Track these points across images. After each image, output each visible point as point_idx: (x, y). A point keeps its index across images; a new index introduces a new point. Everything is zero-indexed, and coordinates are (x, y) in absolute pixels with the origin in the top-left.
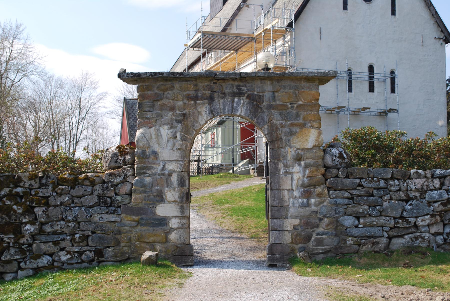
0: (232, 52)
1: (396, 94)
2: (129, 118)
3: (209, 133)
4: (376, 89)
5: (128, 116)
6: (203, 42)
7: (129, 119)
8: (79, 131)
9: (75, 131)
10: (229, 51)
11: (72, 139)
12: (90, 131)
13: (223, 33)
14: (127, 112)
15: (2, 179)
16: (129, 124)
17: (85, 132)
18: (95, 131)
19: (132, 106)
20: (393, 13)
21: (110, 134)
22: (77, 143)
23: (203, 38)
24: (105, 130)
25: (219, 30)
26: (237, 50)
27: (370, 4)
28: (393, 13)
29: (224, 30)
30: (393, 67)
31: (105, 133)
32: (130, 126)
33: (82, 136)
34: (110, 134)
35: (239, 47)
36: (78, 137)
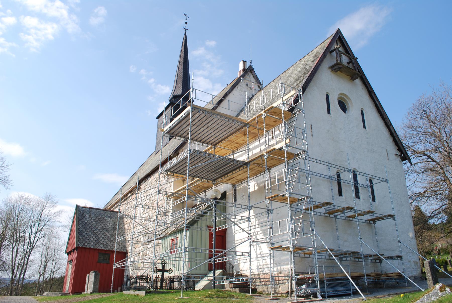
0: (210, 146)
2: (78, 224)
3: (169, 239)
4: (361, 196)
5: (78, 221)
6: (187, 123)
7: (78, 225)
8: (36, 239)
9: (32, 239)
10: (207, 145)
11: (29, 245)
12: (46, 240)
13: (213, 112)
14: (78, 218)
15: (450, 167)
16: (78, 229)
17: (41, 240)
18: (49, 240)
19: (83, 214)
21: (61, 243)
22: (32, 248)
23: (192, 112)
24: (57, 240)
25: (210, 107)
26: (215, 145)
29: (215, 108)
31: (57, 243)
32: (79, 231)
33: (38, 243)
34: (61, 243)
35: (216, 142)
36: (34, 244)
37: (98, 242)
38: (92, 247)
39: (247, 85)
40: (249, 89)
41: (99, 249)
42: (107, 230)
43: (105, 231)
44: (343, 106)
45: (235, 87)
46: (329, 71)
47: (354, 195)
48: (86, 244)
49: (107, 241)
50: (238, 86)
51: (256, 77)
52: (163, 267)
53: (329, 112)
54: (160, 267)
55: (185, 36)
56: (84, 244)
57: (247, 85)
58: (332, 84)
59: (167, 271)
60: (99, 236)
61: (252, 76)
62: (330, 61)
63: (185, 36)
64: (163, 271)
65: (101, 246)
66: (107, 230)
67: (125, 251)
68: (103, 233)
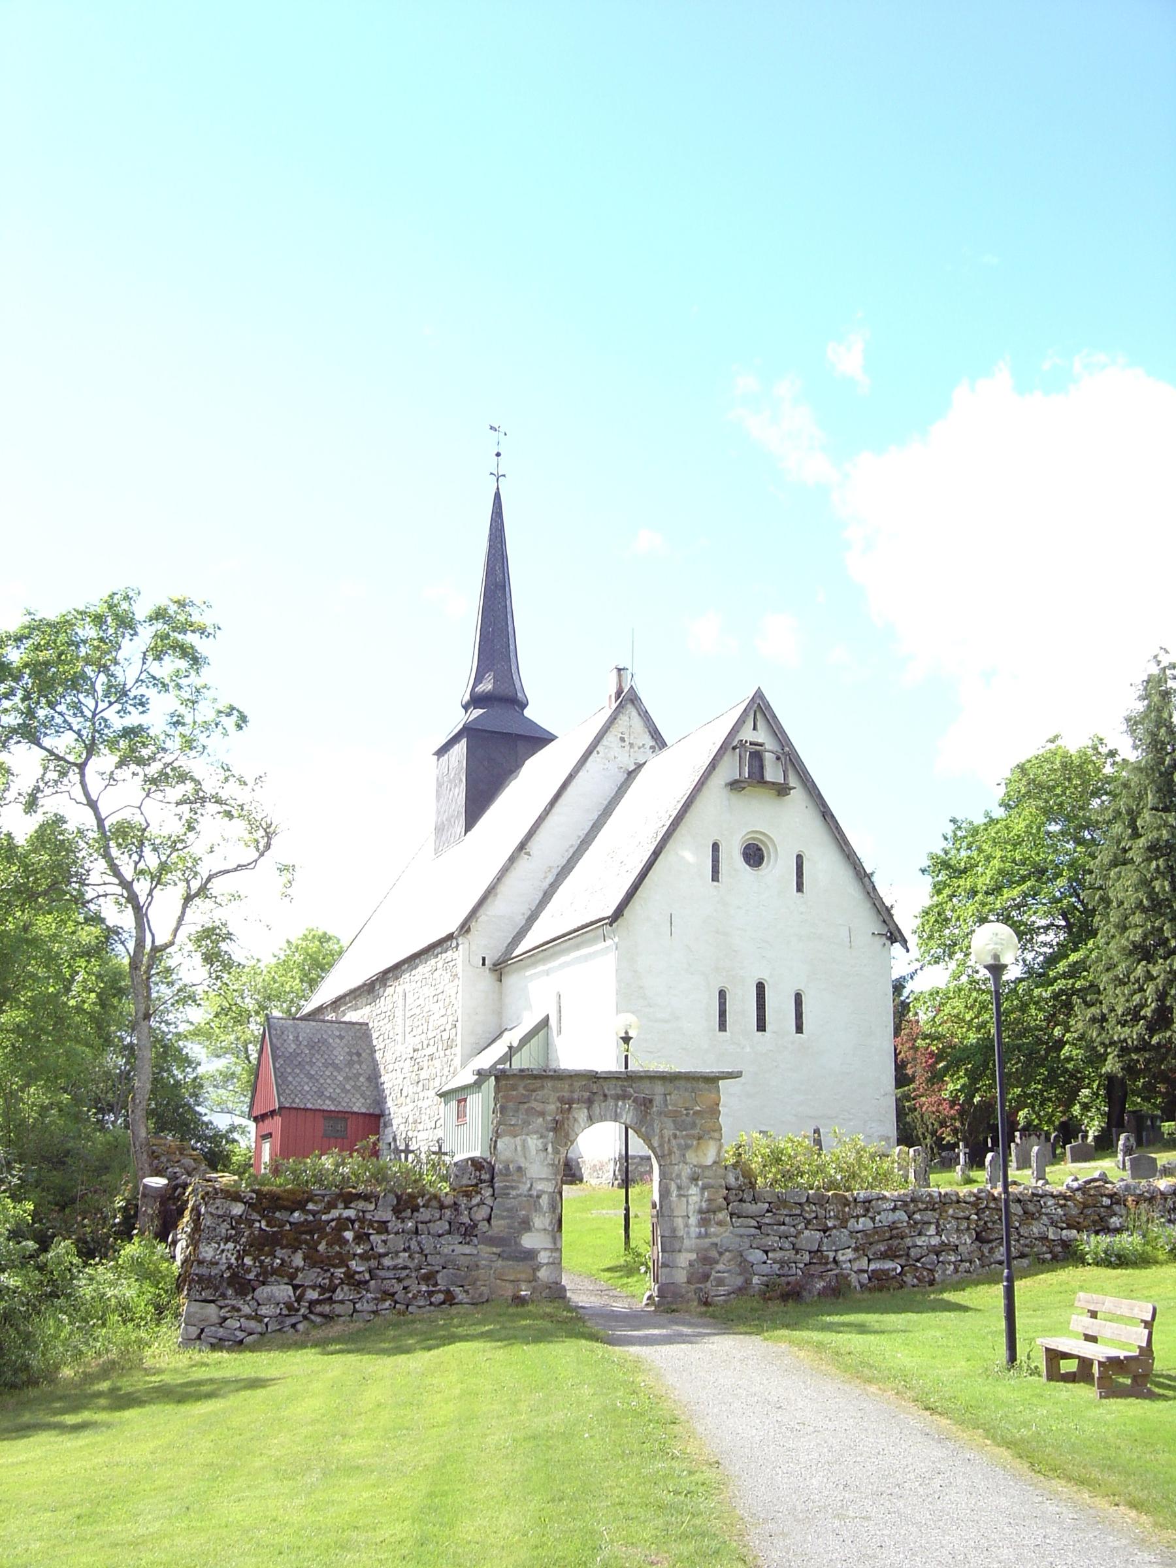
1: (728, 1034)
20: (800, 888)
27: (760, 873)
28: (800, 888)
30: (800, 986)
37: (320, 1094)
38: (309, 1106)
39: (623, 740)
40: (627, 748)
41: (324, 1111)
42: (337, 1068)
43: (330, 1068)
44: (754, 855)
45: (591, 753)
46: (725, 793)
47: (805, 1000)
48: (297, 1100)
49: (338, 1091)
50: (598, 749)
51: (646, 717)
52: (440, 1148)
53: (715, 876)
54: (436, 1149)
55: (497, 496)
56: (293, 1101)
57: (623, 740)
58: (731, 819)
59: (446, 1154)
60: (322, 1081)
61: (634, 713)
62: (729, 769)
63: (497, 496)
64: (440, 1153)
65: (327, 1102)
66: (337, 1068)
67: (377, 1112)
68: (328, 1073)
